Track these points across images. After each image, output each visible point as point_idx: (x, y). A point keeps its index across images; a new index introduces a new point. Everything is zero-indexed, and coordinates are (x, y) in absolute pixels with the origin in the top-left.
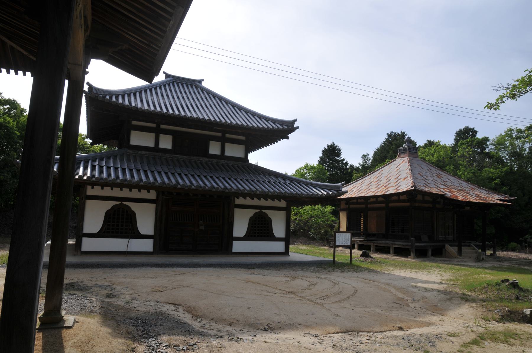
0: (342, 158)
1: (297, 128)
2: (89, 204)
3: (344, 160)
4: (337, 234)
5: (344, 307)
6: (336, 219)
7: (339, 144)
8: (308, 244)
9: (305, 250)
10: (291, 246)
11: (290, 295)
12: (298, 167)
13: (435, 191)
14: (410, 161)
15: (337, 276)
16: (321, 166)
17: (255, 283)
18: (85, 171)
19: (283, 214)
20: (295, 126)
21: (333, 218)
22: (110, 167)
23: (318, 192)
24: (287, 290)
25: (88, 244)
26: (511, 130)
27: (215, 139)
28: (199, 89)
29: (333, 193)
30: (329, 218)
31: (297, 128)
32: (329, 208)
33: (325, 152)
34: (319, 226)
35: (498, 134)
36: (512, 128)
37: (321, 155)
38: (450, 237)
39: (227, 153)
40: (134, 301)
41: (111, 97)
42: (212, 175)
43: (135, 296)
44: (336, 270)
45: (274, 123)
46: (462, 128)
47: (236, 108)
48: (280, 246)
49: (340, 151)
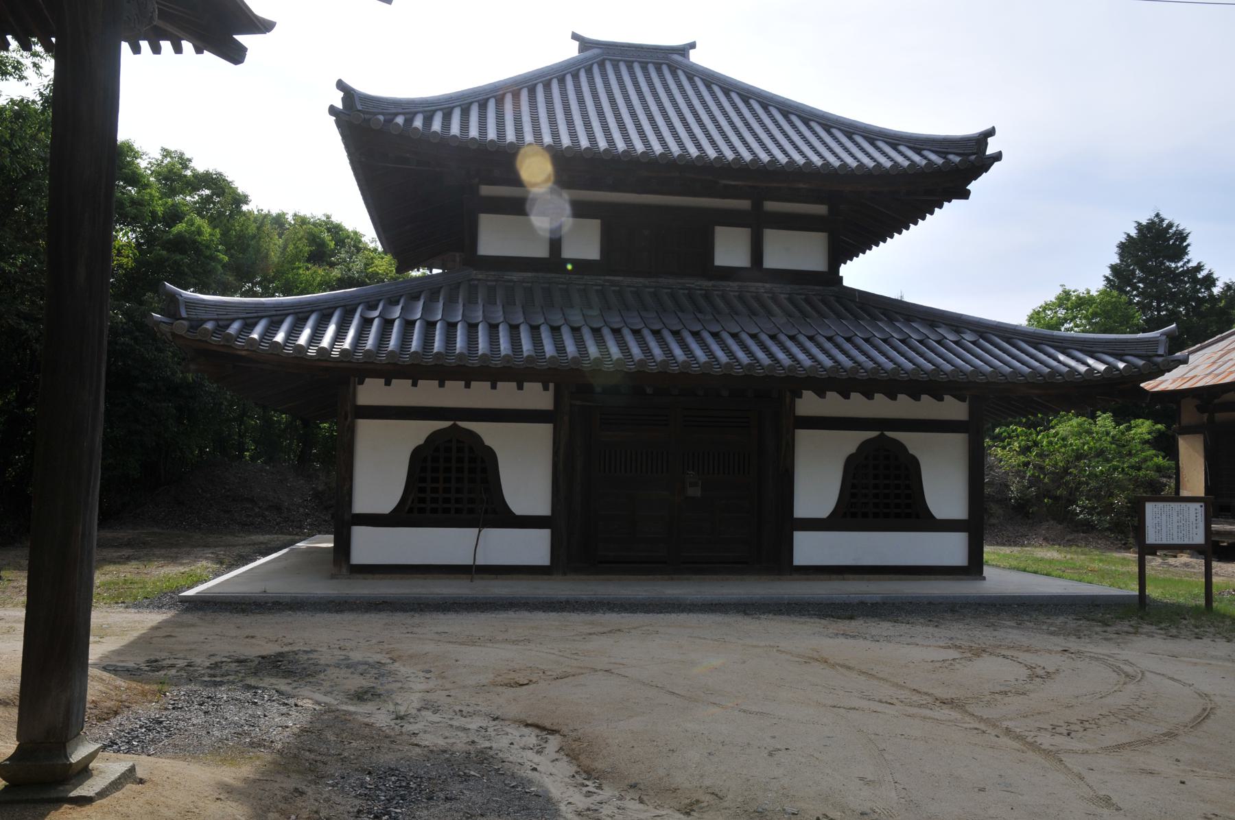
0: (1193, 264)
1: (998, 157)
2: (366, 429)
3: (1199, 268)
4: (1149, 507)
5: (1143, 771)
6: (1172, 463)
7: (1177, 217)
8: (1070, 543)
9: (1051, 561)
10: (987, 549)
11: (945, 713)
12: (1037, 303)
15: (1146, 653)
16: (1115, 293)
17: (833, 666)
18: (340, 335)
19: (957, 443)
20: (990, 151)
21: (1159, 460)
22: (434, 324)
23: (1073, 363)
24: (941, 692)
25: (369, 546)
27: (732, 219)
28: (680, 73)
29: (1130, 365)
30: (1145, 460)
31: (998, 157)
32: (1143, 428)
33: (1127, 248)
34: (1108, 486)
37: (1116, 260)
39: (773, 260)
40: (424, 713)
41: (409, 121)
42: (716, 329)
43: (439, 697)
44: (1147, 628)
45: (918, 151)
47: (794, 118)
48: (949, 549)
49: (1184, 239)
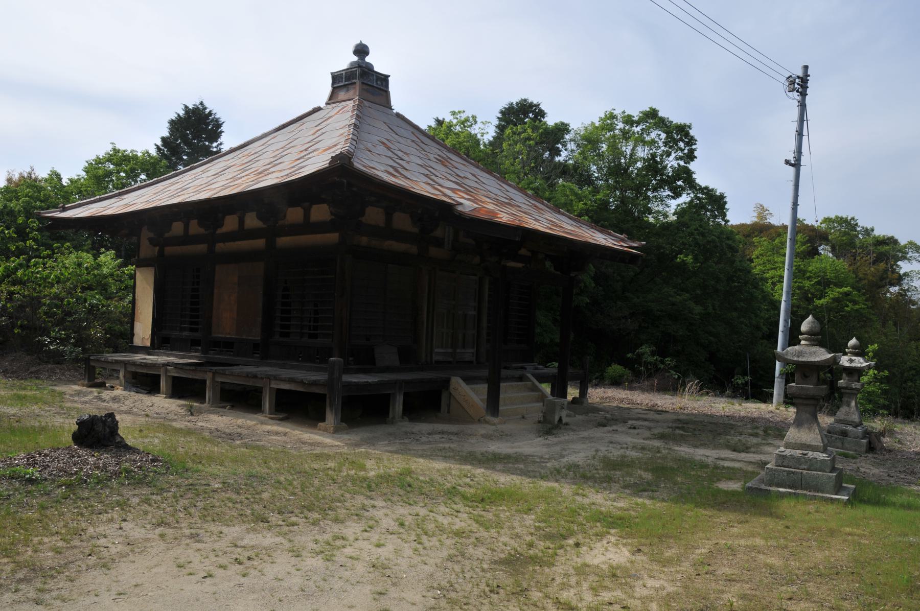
13: (422, 188)
14: (359, 107)
26: (612, 117)
33: (177, 125)
35: (587, 123)
36: (615, 113)
38: (468, 354)
46: (515, 100)
49: (220, 126)
